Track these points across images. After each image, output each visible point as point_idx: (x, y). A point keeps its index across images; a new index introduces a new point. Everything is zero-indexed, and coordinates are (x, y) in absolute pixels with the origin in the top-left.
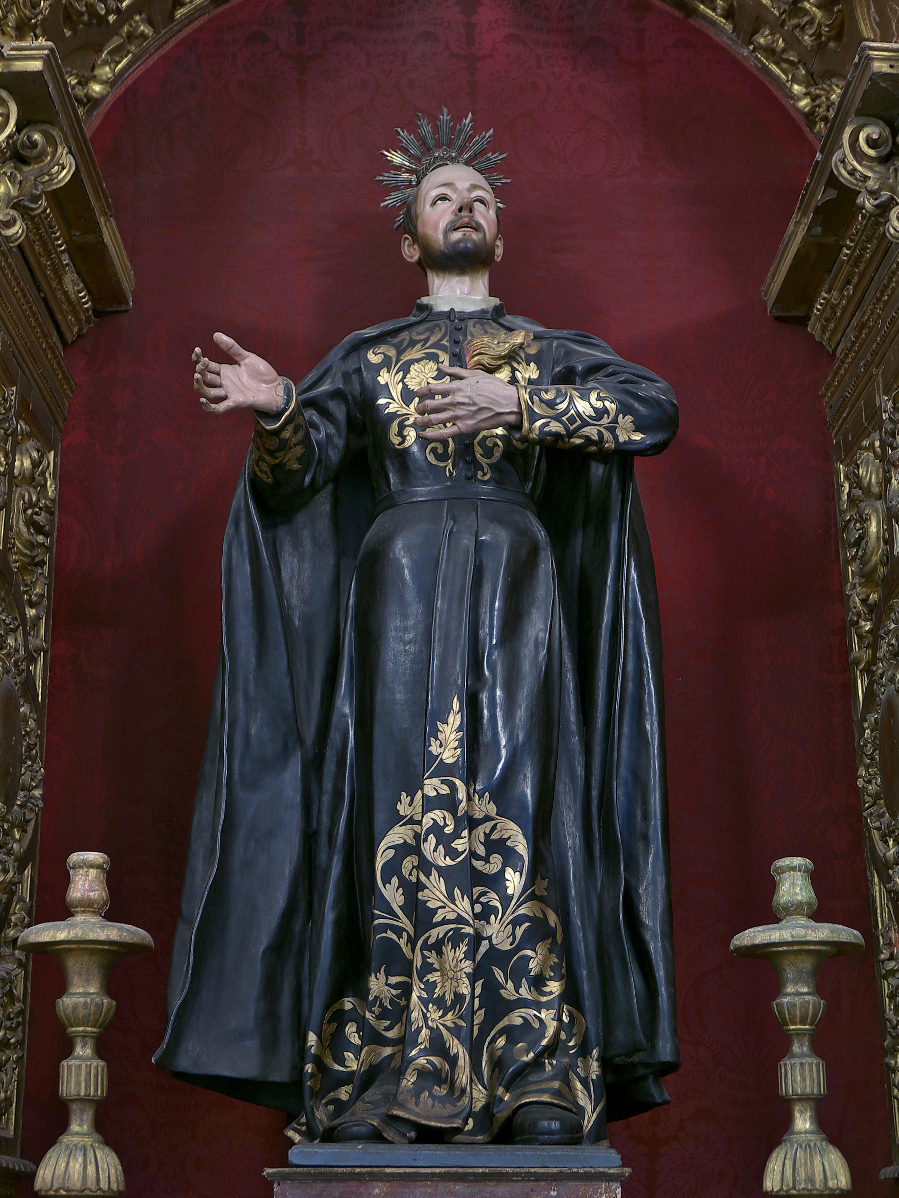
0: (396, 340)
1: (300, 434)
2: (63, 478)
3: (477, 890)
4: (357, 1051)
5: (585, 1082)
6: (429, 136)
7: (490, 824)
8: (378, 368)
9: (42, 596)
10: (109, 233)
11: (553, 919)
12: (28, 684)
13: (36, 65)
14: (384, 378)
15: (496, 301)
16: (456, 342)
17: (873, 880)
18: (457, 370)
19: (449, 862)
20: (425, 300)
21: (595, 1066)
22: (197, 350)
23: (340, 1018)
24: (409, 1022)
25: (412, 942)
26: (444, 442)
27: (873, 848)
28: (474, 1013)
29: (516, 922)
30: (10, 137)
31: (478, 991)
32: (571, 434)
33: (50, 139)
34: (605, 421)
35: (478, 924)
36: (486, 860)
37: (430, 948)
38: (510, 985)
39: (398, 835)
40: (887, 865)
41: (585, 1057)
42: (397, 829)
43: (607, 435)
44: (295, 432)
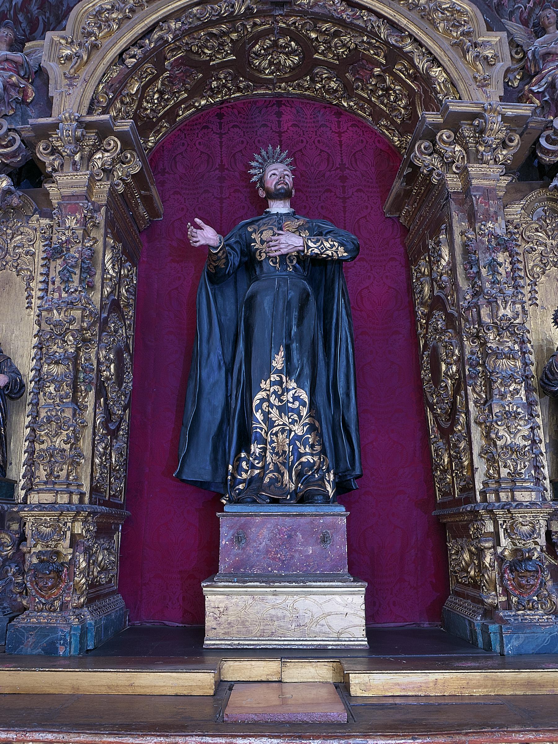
0: (257, 224)
1: (225, 255)
2: (138, 275)
3: (290, 414)
4: (246, 472)
5: (329, 482)
6: (265, 155)
7: (294, 391)
8: (252, 232)
9: (132, 316)
10: (154, 191)
11: (317, 424)
12: (127, 345)
13: (127, 128)
14: (253, 236)
15: (292, 210)
16: (280, 224)
17: (427, 411)
18: (281, 232)
19: (280, 404)
20: (268, 210)
21: (332, 476)
22: (189, 224)
23: (240, 460)
24: (266, 461)
25: (266, 433)
26: (276, 257)
27: (427, 399)
28: (289, 457)
29: (304, 425)
30: (118, 155)
31: (291, 449)
32: (322, 254)
33: (132, 155)
34: (334, 249)
35: (291, 426)
36: (293, 403)
37: (273, 435)
38: (302, 448)
39: (261, 395)
40: (433, 404)
41: (328, 473)
42: (260, 393)
43: (335, 254)
44: (223, 254)
